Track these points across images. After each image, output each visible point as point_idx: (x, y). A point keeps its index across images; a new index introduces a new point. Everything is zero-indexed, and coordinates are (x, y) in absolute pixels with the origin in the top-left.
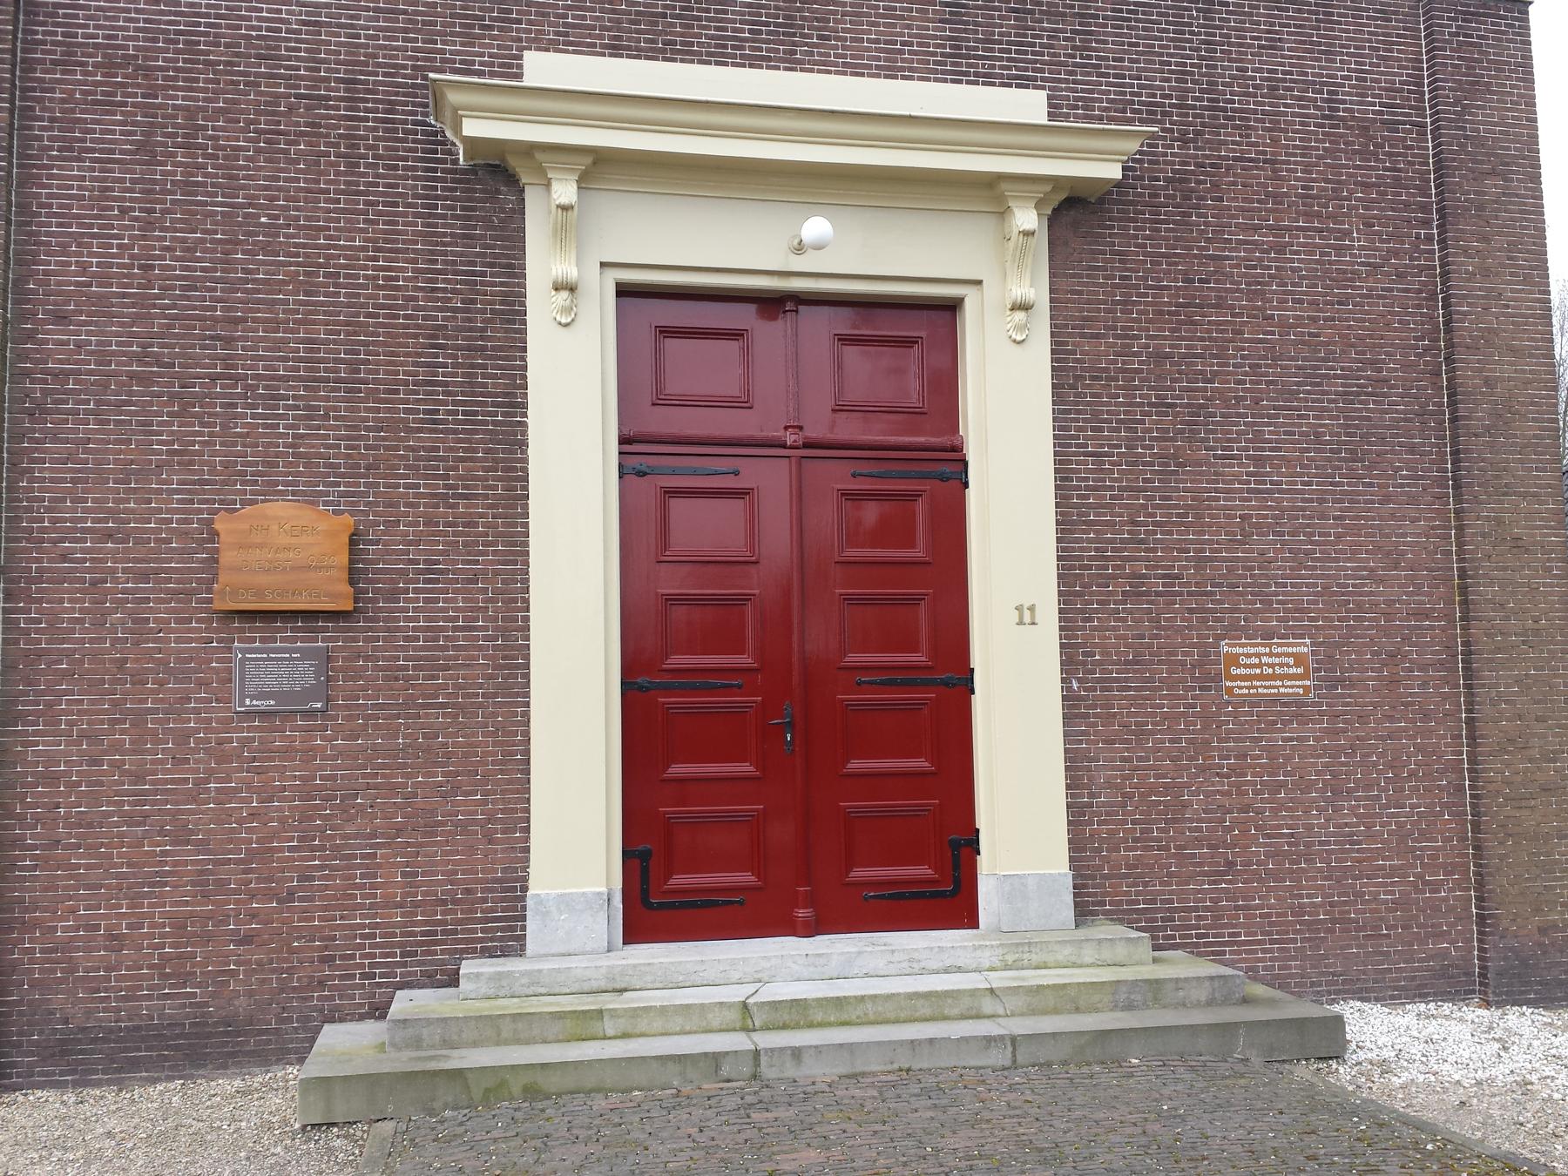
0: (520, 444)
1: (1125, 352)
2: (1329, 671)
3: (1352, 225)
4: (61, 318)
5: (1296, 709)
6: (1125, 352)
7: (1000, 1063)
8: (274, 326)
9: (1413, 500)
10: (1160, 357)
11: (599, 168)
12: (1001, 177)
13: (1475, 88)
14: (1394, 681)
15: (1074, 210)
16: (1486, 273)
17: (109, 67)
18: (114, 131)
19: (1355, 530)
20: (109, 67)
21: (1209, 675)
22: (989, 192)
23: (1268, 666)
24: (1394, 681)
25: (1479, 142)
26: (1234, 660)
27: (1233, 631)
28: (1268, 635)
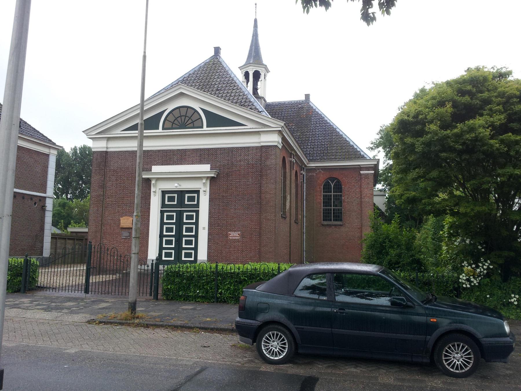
0: (149, 209)
1: (219, 196)
2: (242, 236)
3: (250, 178)
4: (108, 198)
5: (238, 241)
6: (219, 196)
7: (230, 328)
8: (127, 197)
9: (256, 214)
10: (223, 196)
11: (158, 179)
12: (259, 131)
13: (267, 158)
14: (251, 237)
15: (212, 180)
16: (266, 183)
17: (113, 171)
18: (114, 178)
19: (247, 218)
21: (227, 236)
22: (200, 178)
23: (234, 235)
24: (251, 237)
25: (267, 166)
26: (230, 234)
27: (230, 231)
28: (235, 231)
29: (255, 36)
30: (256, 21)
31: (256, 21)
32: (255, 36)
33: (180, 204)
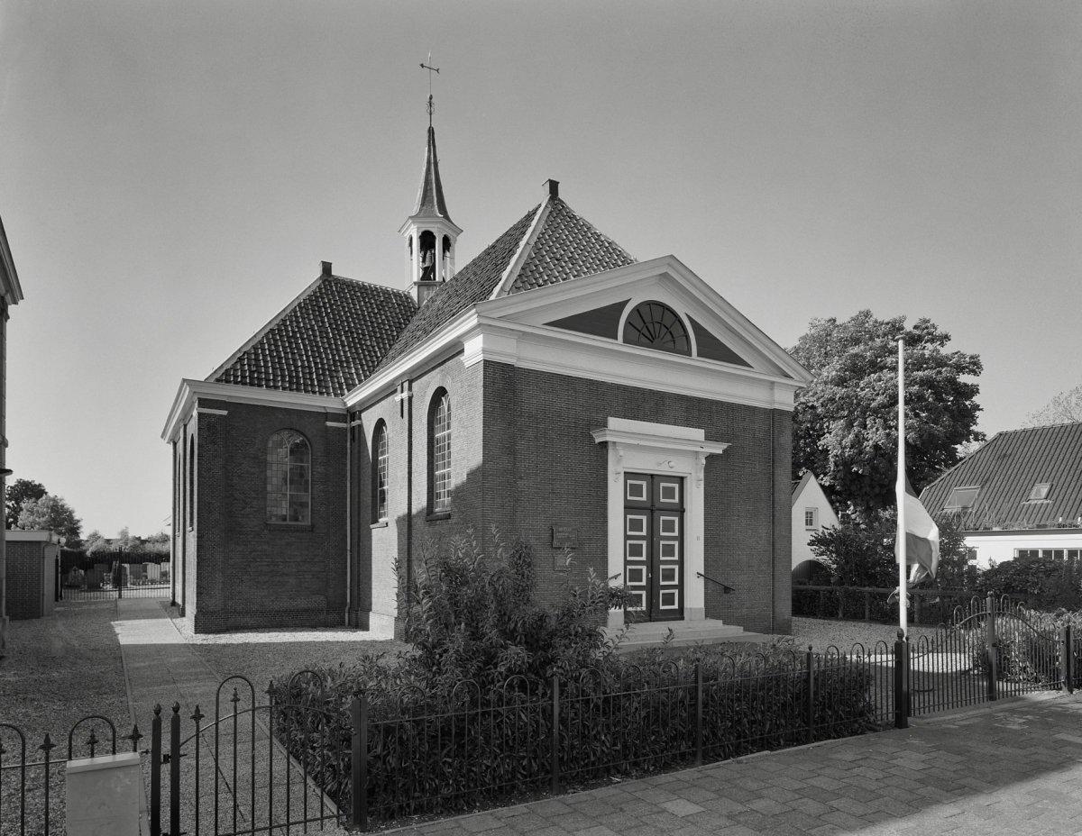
4: (521, 478)
20: (529, 417)
29: (433, 164)
30: (431, 132)
31: (431, 132)
32: (433, 164)
33: (655, 502)
